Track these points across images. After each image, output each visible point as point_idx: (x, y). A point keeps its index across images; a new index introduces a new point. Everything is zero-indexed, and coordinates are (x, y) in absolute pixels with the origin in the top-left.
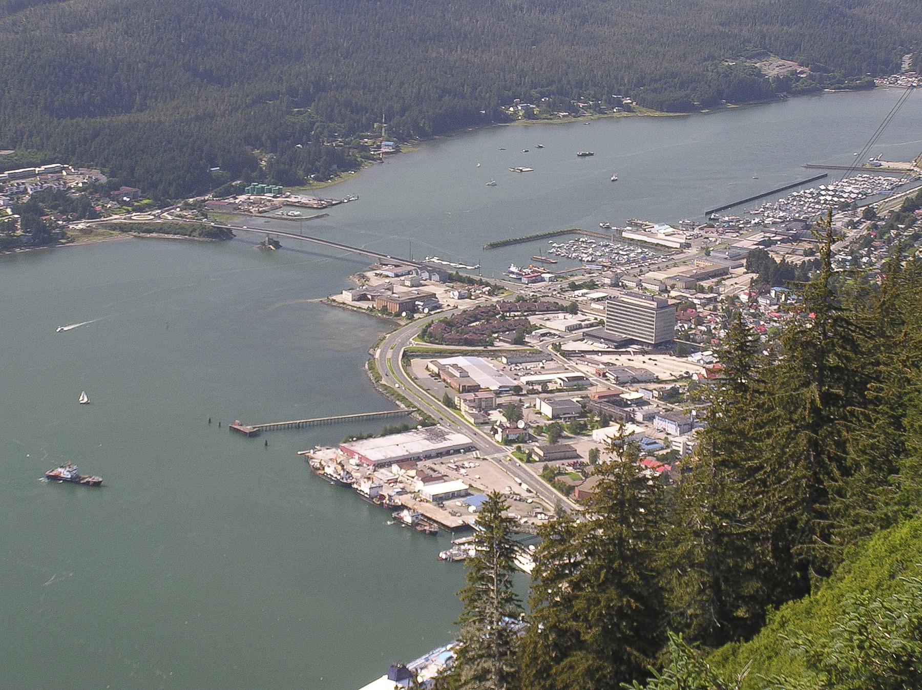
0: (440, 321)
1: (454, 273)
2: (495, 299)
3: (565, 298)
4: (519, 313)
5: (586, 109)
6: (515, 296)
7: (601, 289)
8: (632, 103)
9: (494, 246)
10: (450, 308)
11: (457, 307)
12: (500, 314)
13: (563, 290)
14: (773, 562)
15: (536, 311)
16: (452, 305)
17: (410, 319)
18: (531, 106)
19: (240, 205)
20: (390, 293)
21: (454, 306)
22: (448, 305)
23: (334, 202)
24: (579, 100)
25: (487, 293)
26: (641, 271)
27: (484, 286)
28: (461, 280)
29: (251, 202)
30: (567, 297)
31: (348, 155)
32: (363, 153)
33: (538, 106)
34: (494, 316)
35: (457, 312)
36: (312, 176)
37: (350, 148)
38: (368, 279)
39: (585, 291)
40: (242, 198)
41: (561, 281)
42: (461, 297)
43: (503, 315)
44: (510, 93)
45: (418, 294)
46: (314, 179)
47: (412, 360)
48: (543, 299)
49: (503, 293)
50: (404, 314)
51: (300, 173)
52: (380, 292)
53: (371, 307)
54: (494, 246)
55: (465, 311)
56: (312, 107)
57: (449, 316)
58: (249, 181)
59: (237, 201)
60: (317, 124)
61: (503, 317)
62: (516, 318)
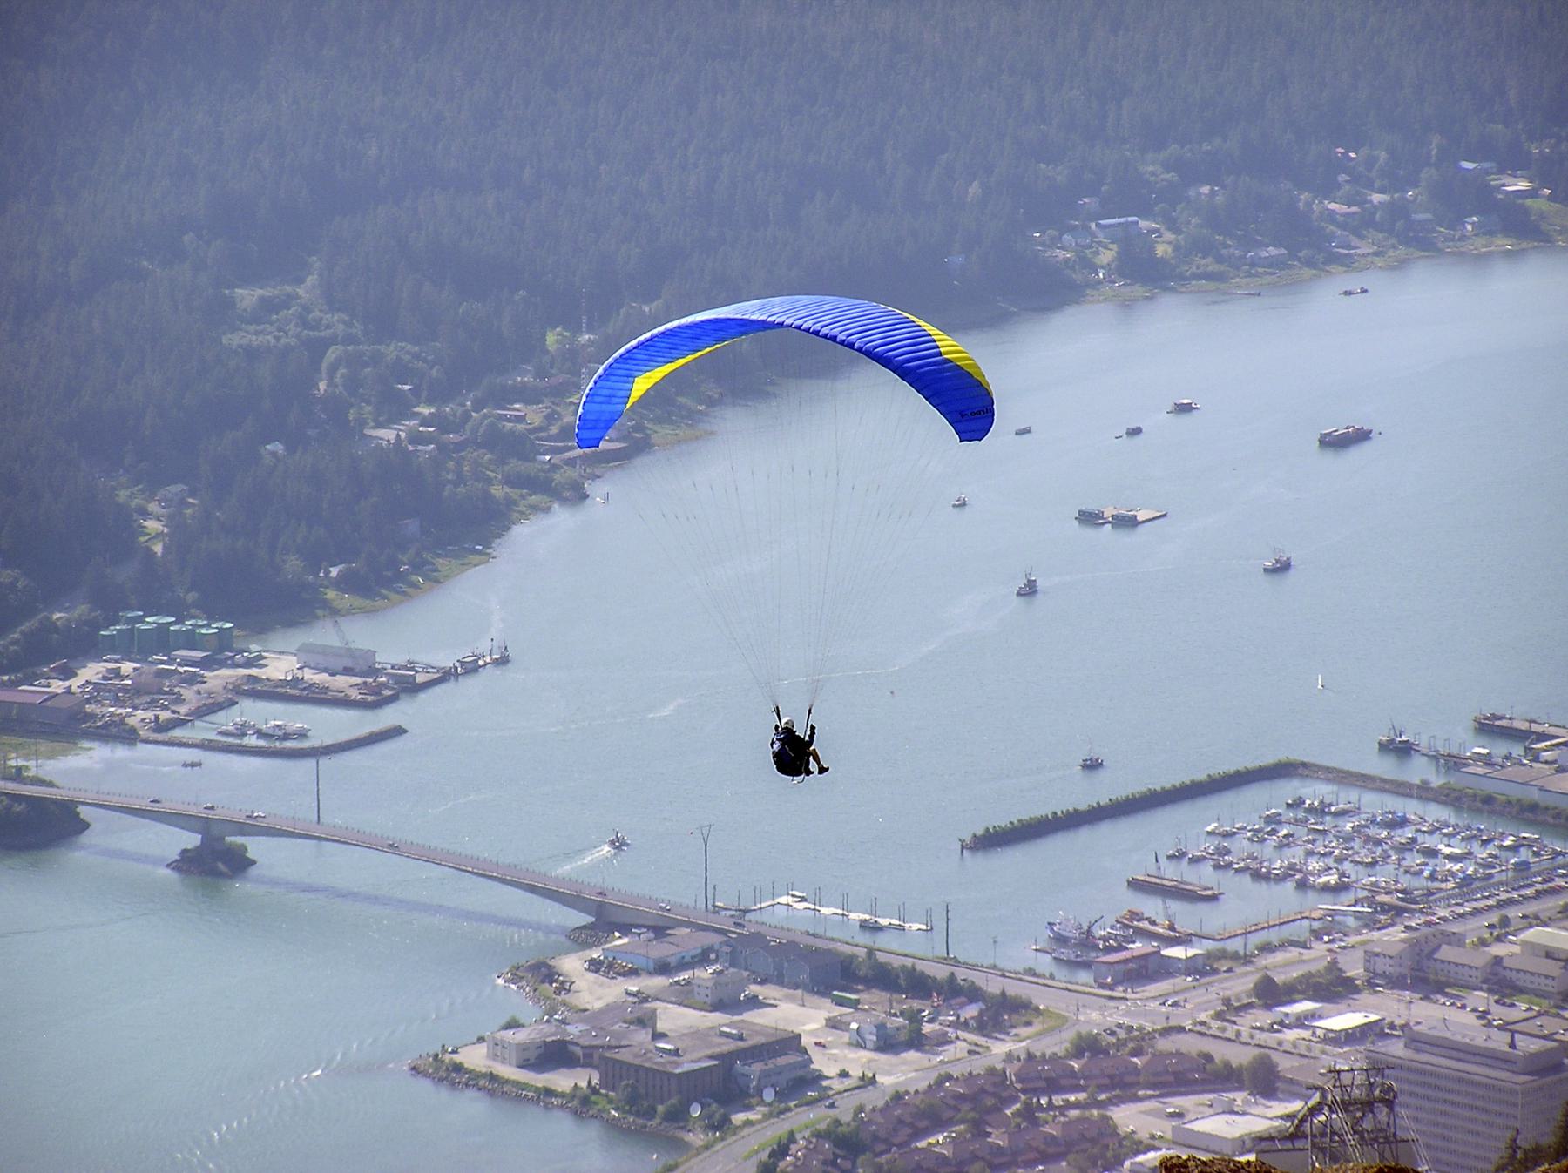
0: (818, 1135)
1: (862, 952)
2: (1000, 1048)
3: (1238, 1034)
4: (1082, 1096)
5: (1363, 224)
6: (1068, 1035)
7: (1365, 997)
8: (1531, 194)
9: (991, 841)
10: (848, 1083)
11: (873, 1081)
12: (1016, 1099)
13: (1230, 1010)
14: (16, 677)
15: (1137, 1085)
16: (856, 1072)
17: (714, 1128)
18: (1144, 224)
19: (88, 701)
20: (642, 1036)
21: (863, 1078)
22: (844, 1074)
23: (420, 678)
24: (1328, 191)
25: (972, 1023)
26: (1505, 922)
27: (963, 999)
28: (884, 978)
29: (125, 689)
30: (1245, 1031)
31: (460, 479)
32: (515, 465)
33: (1173, 226)
34: (998, 1109)
35: (873, 1099)
36: (334, 572)
37: (460, 447)
38: (564, 987)
39: (1307, 1006)
40: (92, 672)
41: (1230, 970)
42: (888, 1044)
43: (1027, 1106)
44: (1061, 175)
45: (741, 1038)
46: (343, 584)
47: (200, 836)
48: (1163, 1045)
49: (1029, 1024)
50: (696, 1111)
51: (293, 564)
52: (612, 1034)
53: (584, 1084)
54: (991, 841)
55: (898, 1097)
56: (311, 280)
57: (844, 1111)
58: (110, 603)
59: (75, 683)
60: (332, 354)
61: (1029, 1113)
62: (1074, 1113)
